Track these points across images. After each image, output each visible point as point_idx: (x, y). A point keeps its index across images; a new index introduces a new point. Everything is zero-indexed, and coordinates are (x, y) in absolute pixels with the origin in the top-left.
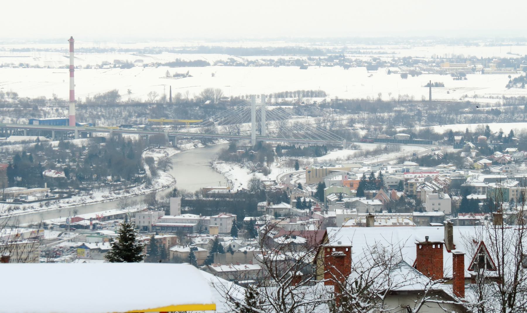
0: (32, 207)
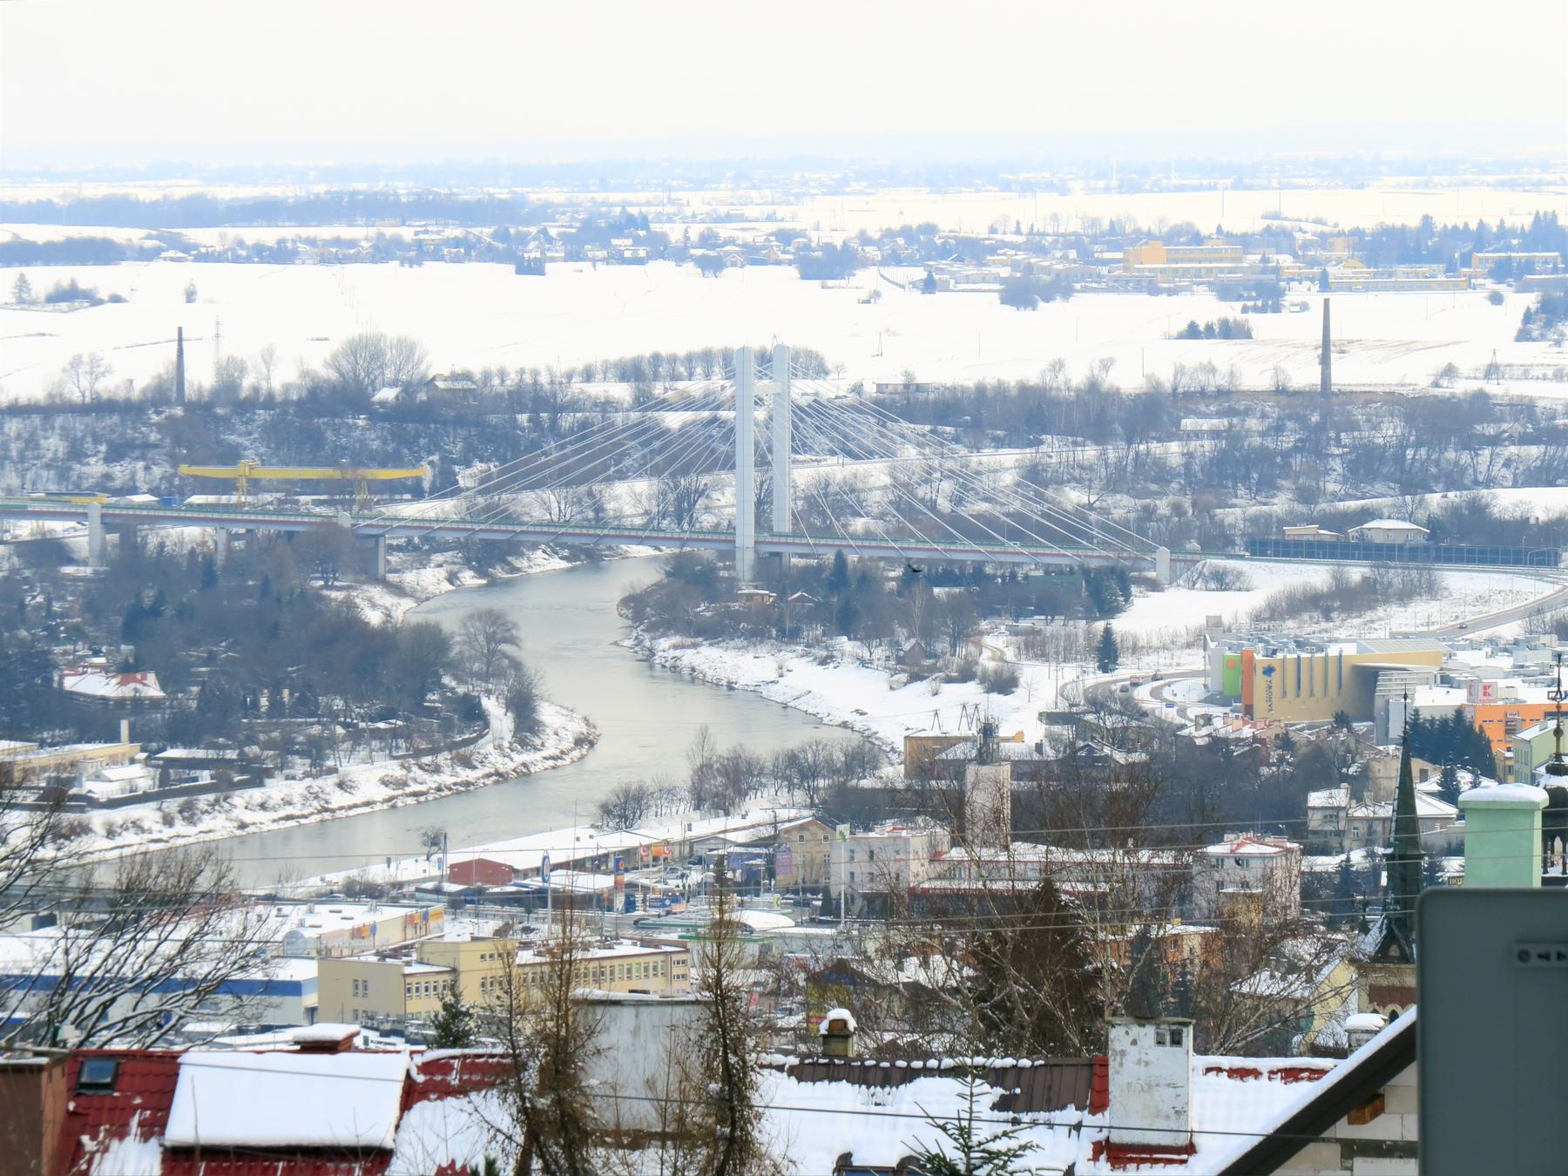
0: (137, 826)
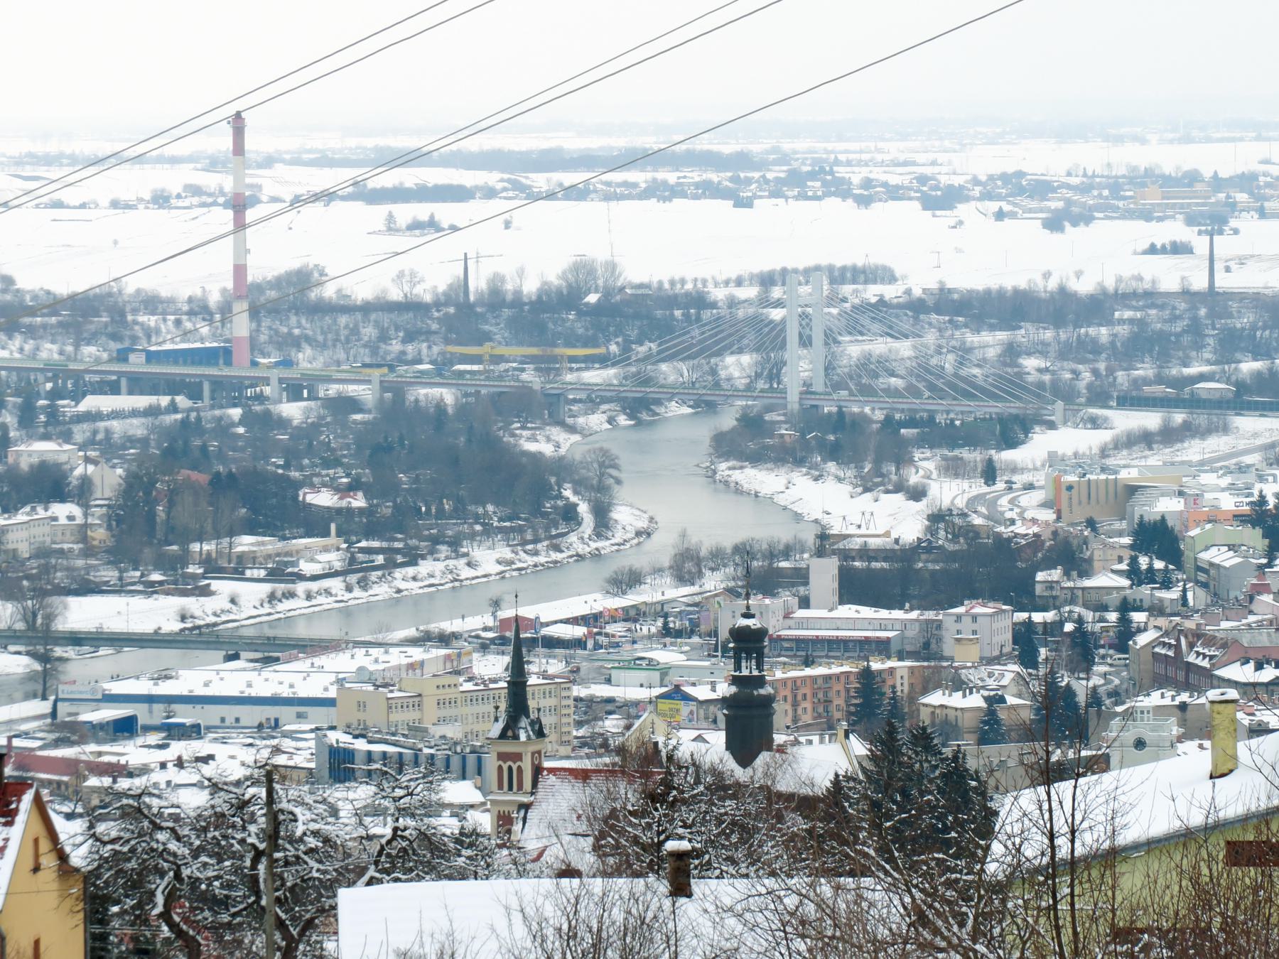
0: (328, 592)
